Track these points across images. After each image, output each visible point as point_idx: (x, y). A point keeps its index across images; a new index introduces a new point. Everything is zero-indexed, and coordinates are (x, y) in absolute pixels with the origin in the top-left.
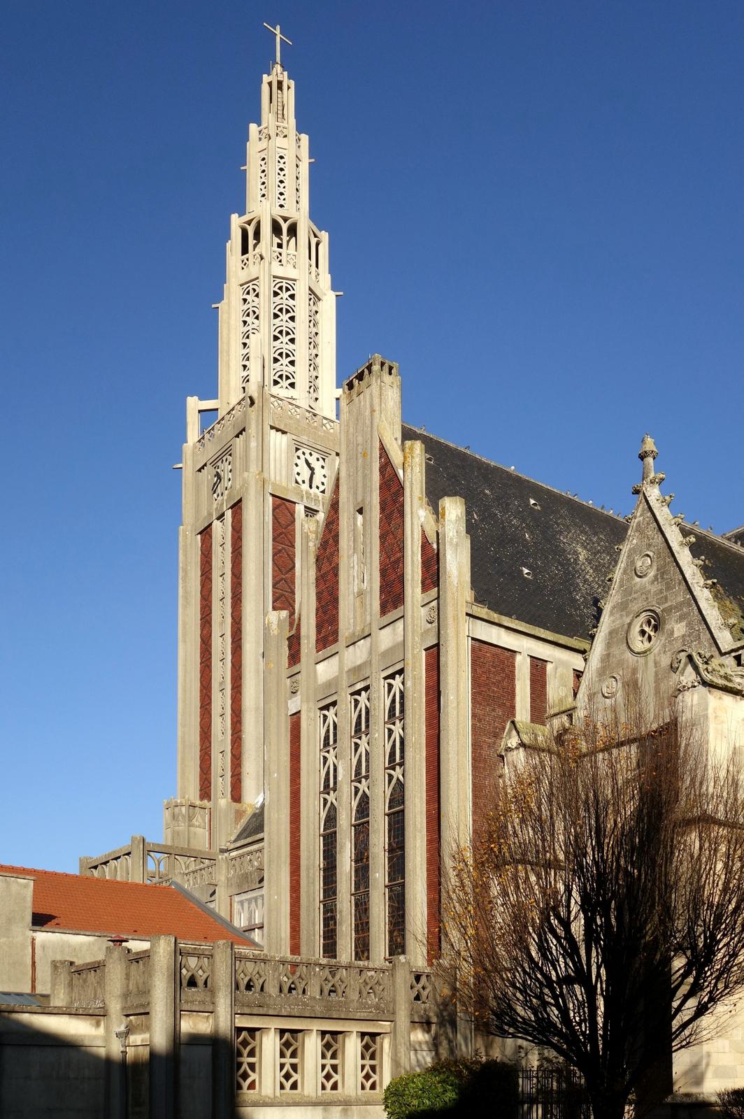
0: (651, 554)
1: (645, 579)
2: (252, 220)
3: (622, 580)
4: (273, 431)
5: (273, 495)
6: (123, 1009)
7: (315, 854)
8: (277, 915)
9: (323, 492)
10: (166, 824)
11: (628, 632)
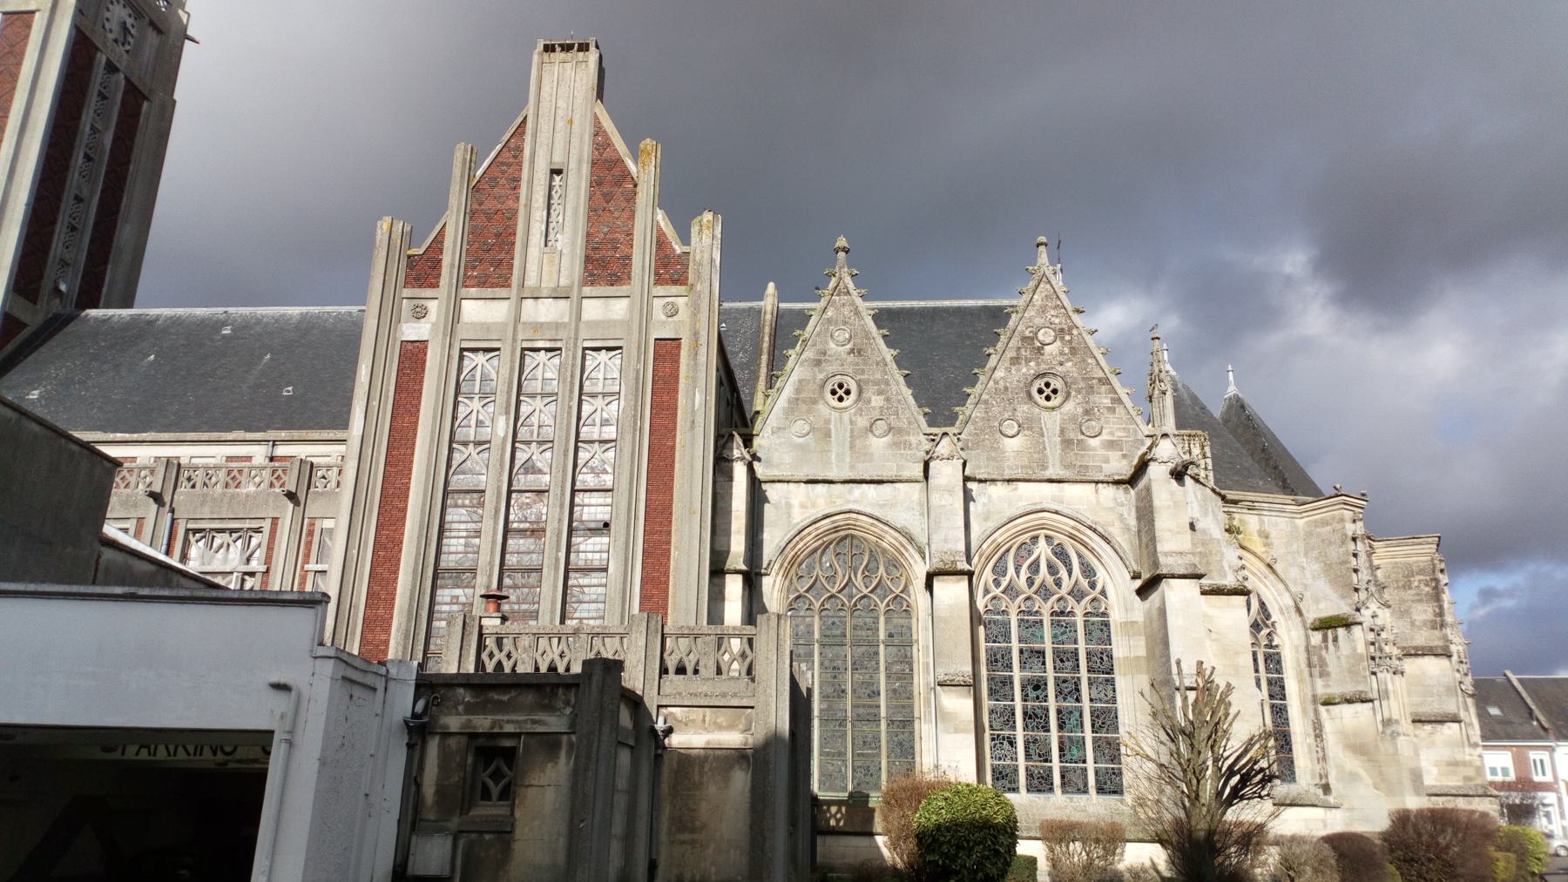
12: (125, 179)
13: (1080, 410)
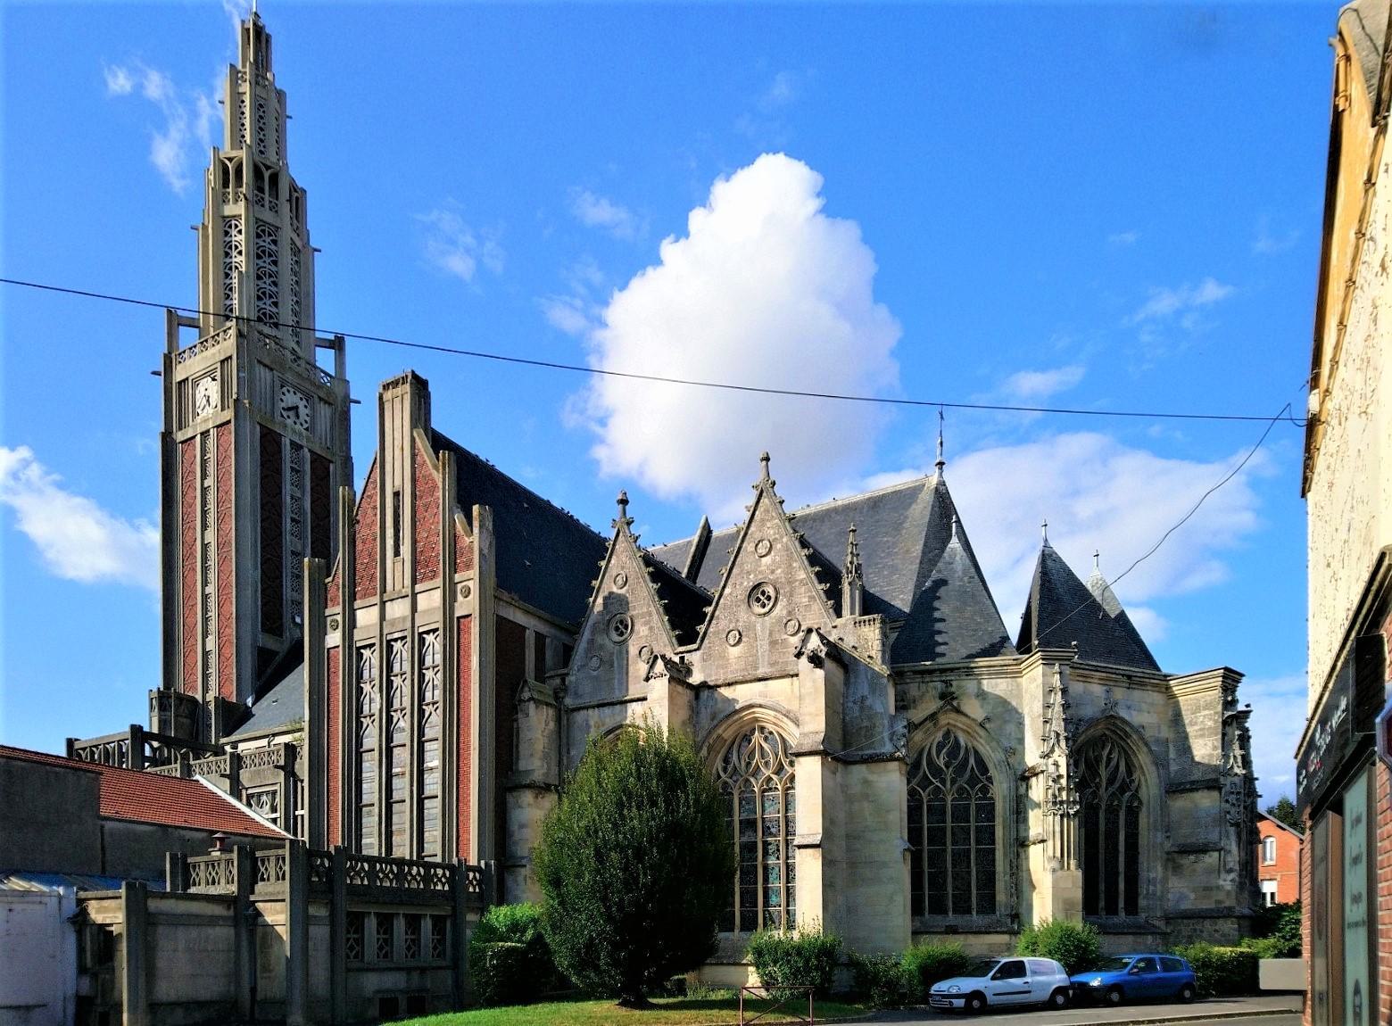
13: (785, 612)
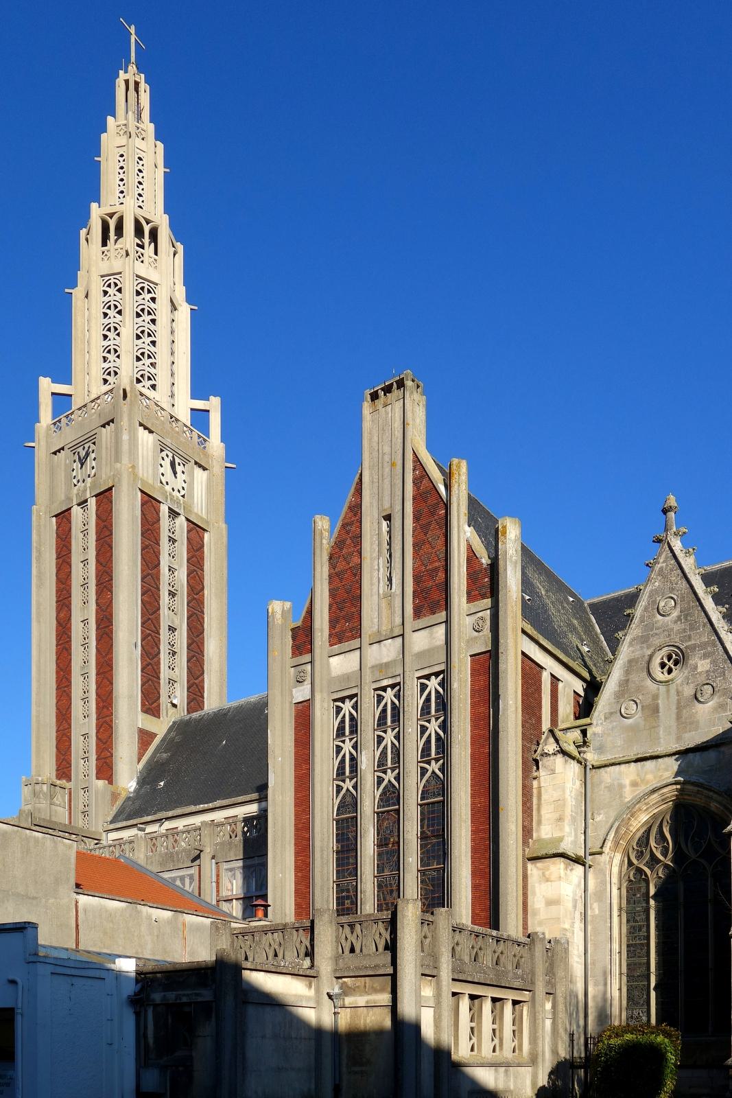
0: (675, 597)
1: (667, 618)
2: (116, 213)
3: (642, 617)
4: (142, 428)
5: (142, 491)
6: (335, 970)
7: (329, 837)
8: (282, 893)
9: (183, 496)
10: (25, 800)
11: (649, 663)
12: (203, 603)
